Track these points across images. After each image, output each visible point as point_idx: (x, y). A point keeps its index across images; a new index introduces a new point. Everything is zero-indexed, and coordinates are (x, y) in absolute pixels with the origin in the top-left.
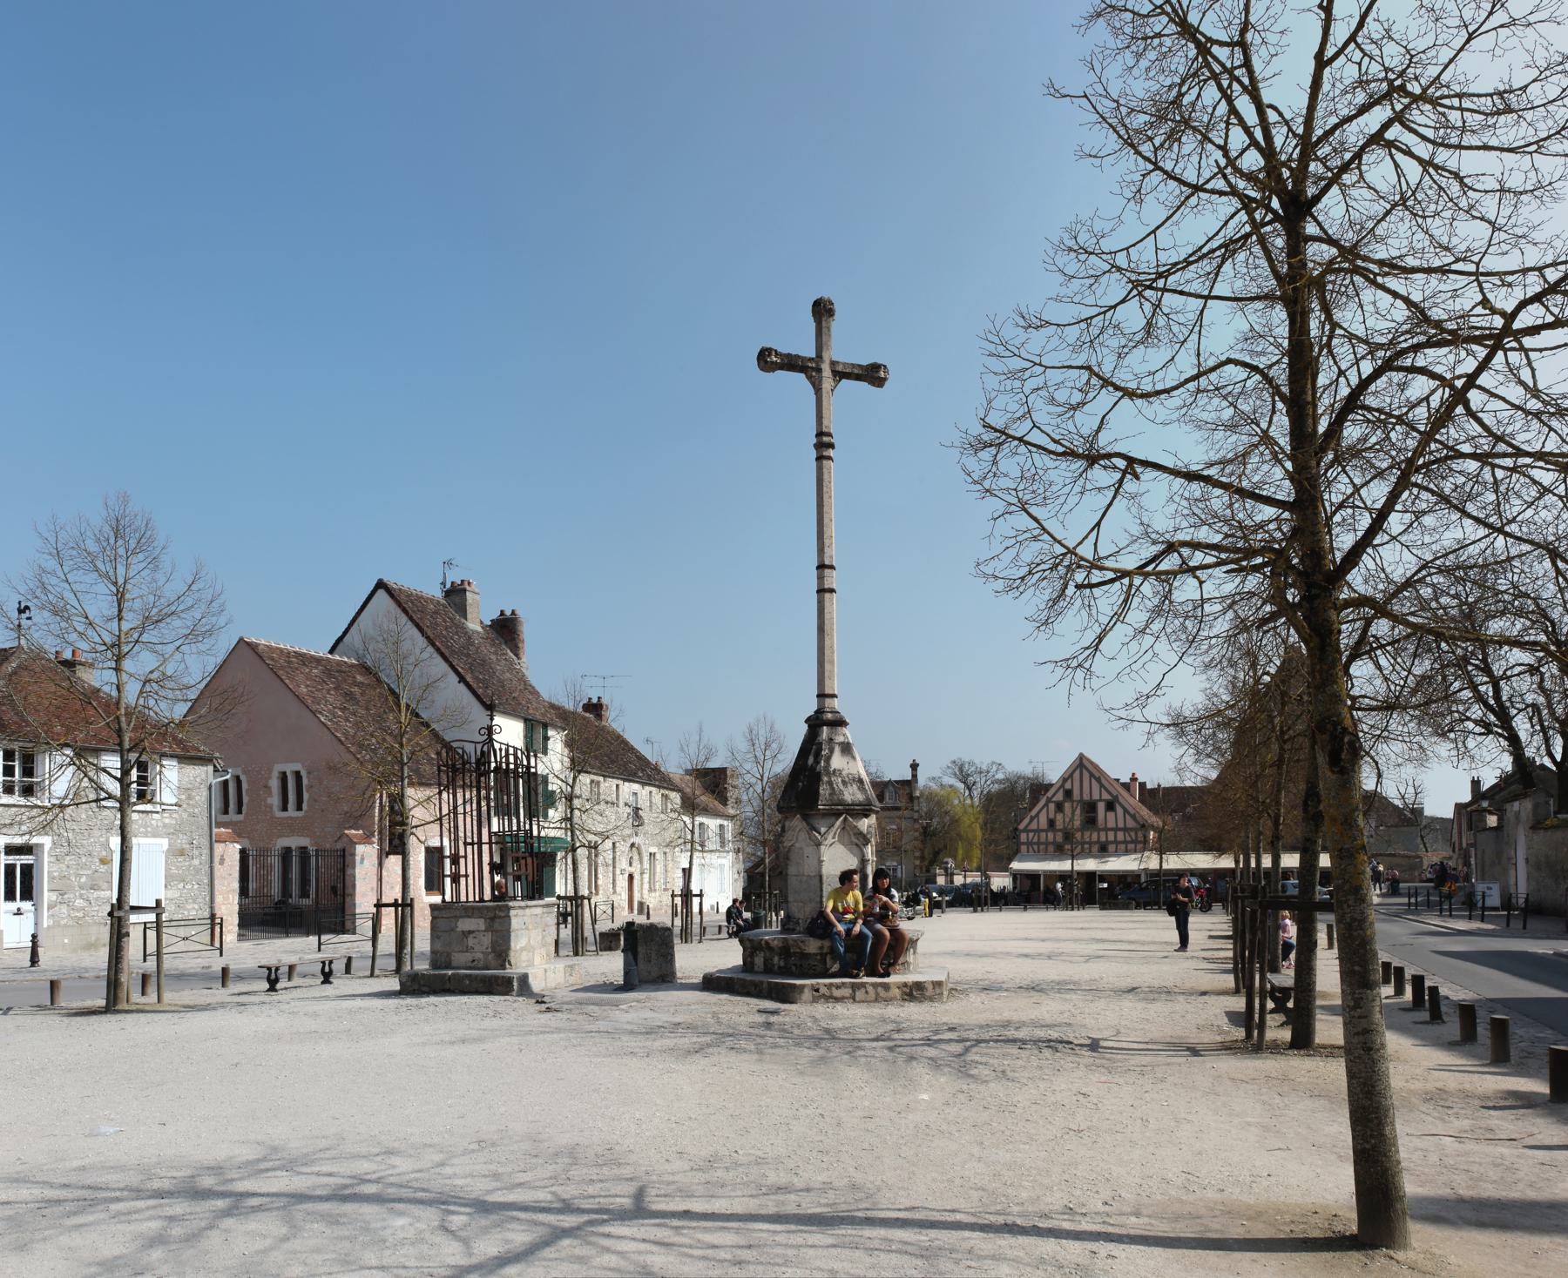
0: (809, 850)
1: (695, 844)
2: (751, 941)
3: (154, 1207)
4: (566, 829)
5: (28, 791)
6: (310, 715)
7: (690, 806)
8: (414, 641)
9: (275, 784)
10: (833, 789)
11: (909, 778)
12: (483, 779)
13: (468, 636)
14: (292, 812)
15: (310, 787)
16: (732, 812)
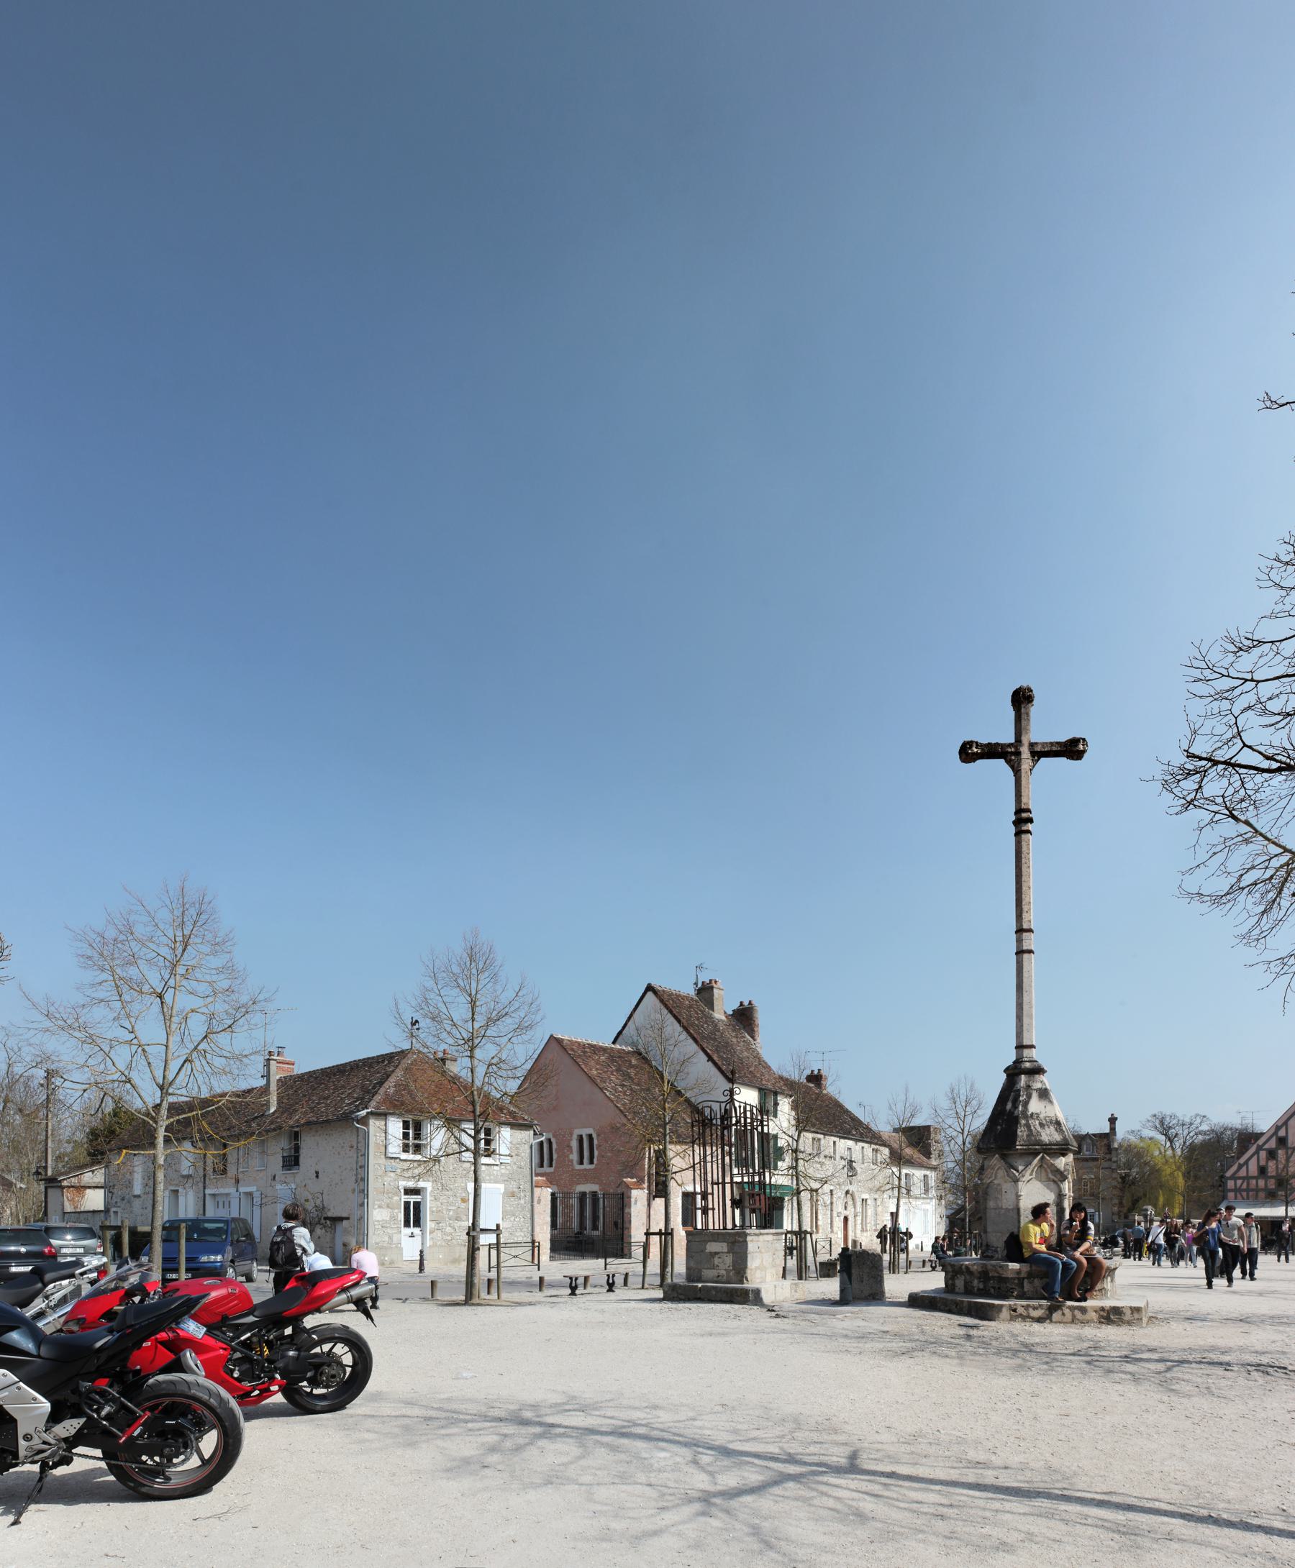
0: (1007, 1186)
1: (902, 1190)
2: (953, 1266)
3: (496, 1427)
4: (792, 1176)
5: (418, 1149)
6: (597, 1090)
7: (897, 1158)
8: (673, 1028)
9: (574, 1144)
10: (1030, 1130)
11: (1107, 1130)
12: (726, 1132)
13: (715, 1024)
14: (586, 1166)
15: (599, 1146)
16: (934, 1163)
